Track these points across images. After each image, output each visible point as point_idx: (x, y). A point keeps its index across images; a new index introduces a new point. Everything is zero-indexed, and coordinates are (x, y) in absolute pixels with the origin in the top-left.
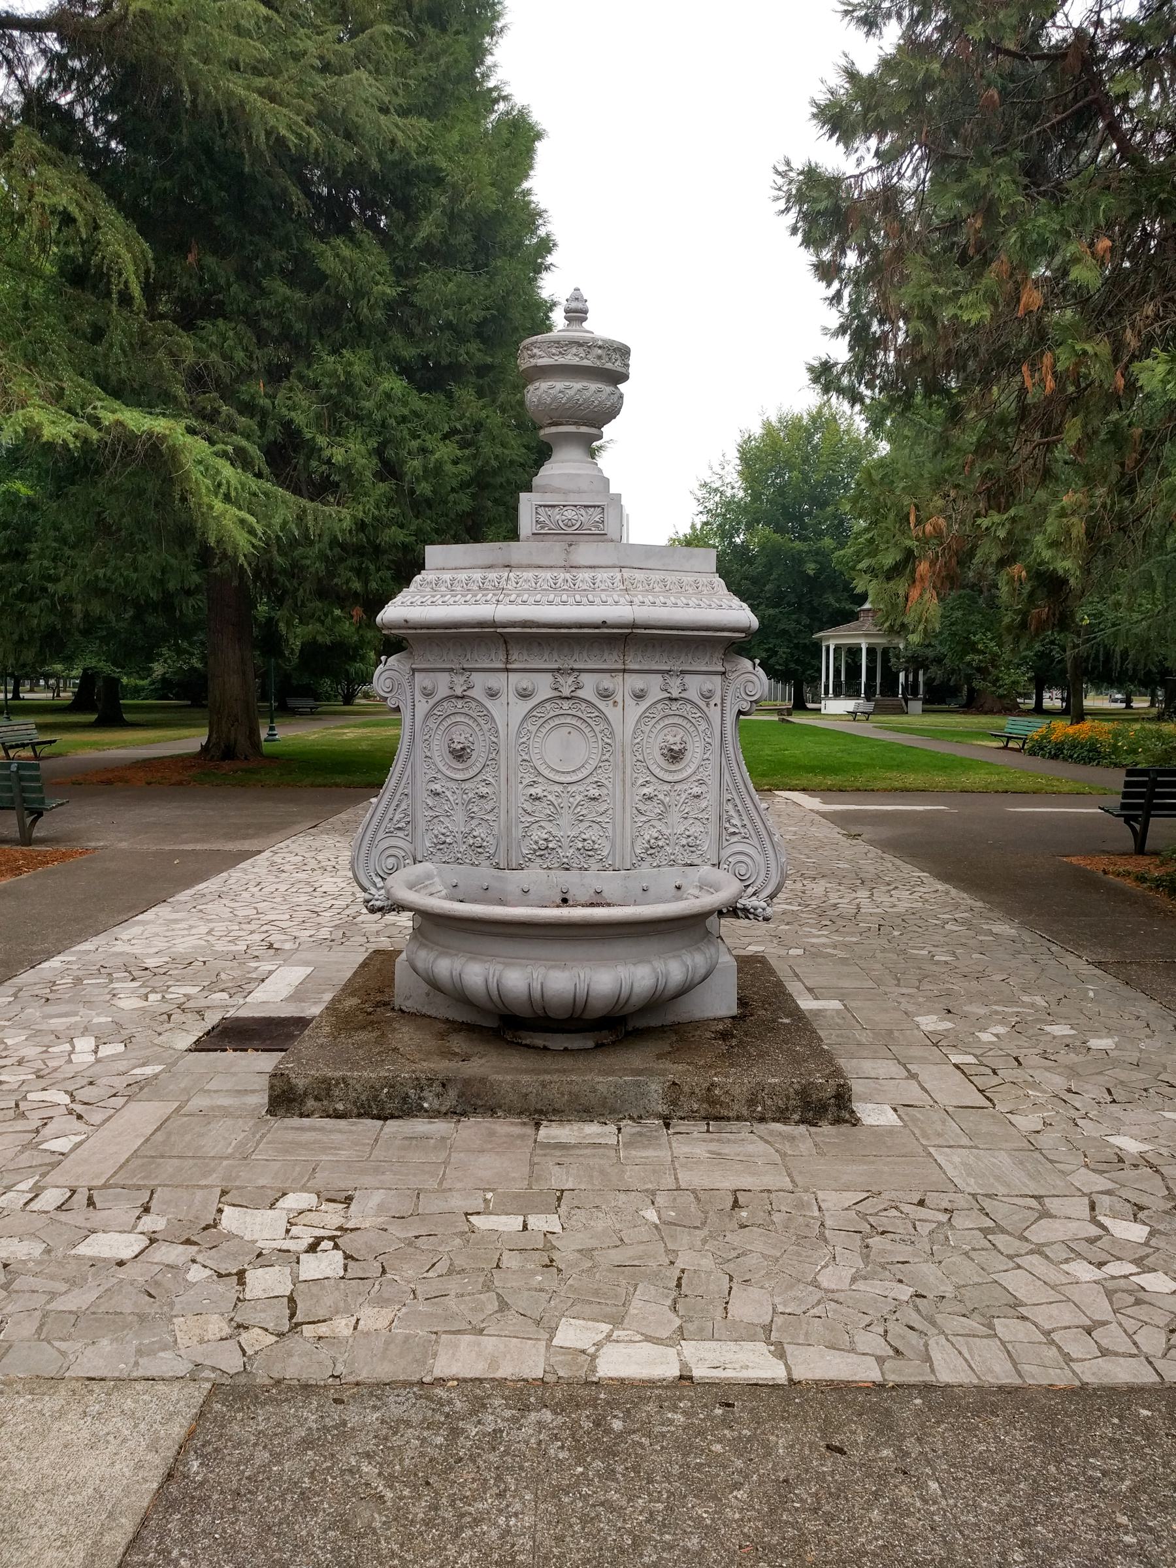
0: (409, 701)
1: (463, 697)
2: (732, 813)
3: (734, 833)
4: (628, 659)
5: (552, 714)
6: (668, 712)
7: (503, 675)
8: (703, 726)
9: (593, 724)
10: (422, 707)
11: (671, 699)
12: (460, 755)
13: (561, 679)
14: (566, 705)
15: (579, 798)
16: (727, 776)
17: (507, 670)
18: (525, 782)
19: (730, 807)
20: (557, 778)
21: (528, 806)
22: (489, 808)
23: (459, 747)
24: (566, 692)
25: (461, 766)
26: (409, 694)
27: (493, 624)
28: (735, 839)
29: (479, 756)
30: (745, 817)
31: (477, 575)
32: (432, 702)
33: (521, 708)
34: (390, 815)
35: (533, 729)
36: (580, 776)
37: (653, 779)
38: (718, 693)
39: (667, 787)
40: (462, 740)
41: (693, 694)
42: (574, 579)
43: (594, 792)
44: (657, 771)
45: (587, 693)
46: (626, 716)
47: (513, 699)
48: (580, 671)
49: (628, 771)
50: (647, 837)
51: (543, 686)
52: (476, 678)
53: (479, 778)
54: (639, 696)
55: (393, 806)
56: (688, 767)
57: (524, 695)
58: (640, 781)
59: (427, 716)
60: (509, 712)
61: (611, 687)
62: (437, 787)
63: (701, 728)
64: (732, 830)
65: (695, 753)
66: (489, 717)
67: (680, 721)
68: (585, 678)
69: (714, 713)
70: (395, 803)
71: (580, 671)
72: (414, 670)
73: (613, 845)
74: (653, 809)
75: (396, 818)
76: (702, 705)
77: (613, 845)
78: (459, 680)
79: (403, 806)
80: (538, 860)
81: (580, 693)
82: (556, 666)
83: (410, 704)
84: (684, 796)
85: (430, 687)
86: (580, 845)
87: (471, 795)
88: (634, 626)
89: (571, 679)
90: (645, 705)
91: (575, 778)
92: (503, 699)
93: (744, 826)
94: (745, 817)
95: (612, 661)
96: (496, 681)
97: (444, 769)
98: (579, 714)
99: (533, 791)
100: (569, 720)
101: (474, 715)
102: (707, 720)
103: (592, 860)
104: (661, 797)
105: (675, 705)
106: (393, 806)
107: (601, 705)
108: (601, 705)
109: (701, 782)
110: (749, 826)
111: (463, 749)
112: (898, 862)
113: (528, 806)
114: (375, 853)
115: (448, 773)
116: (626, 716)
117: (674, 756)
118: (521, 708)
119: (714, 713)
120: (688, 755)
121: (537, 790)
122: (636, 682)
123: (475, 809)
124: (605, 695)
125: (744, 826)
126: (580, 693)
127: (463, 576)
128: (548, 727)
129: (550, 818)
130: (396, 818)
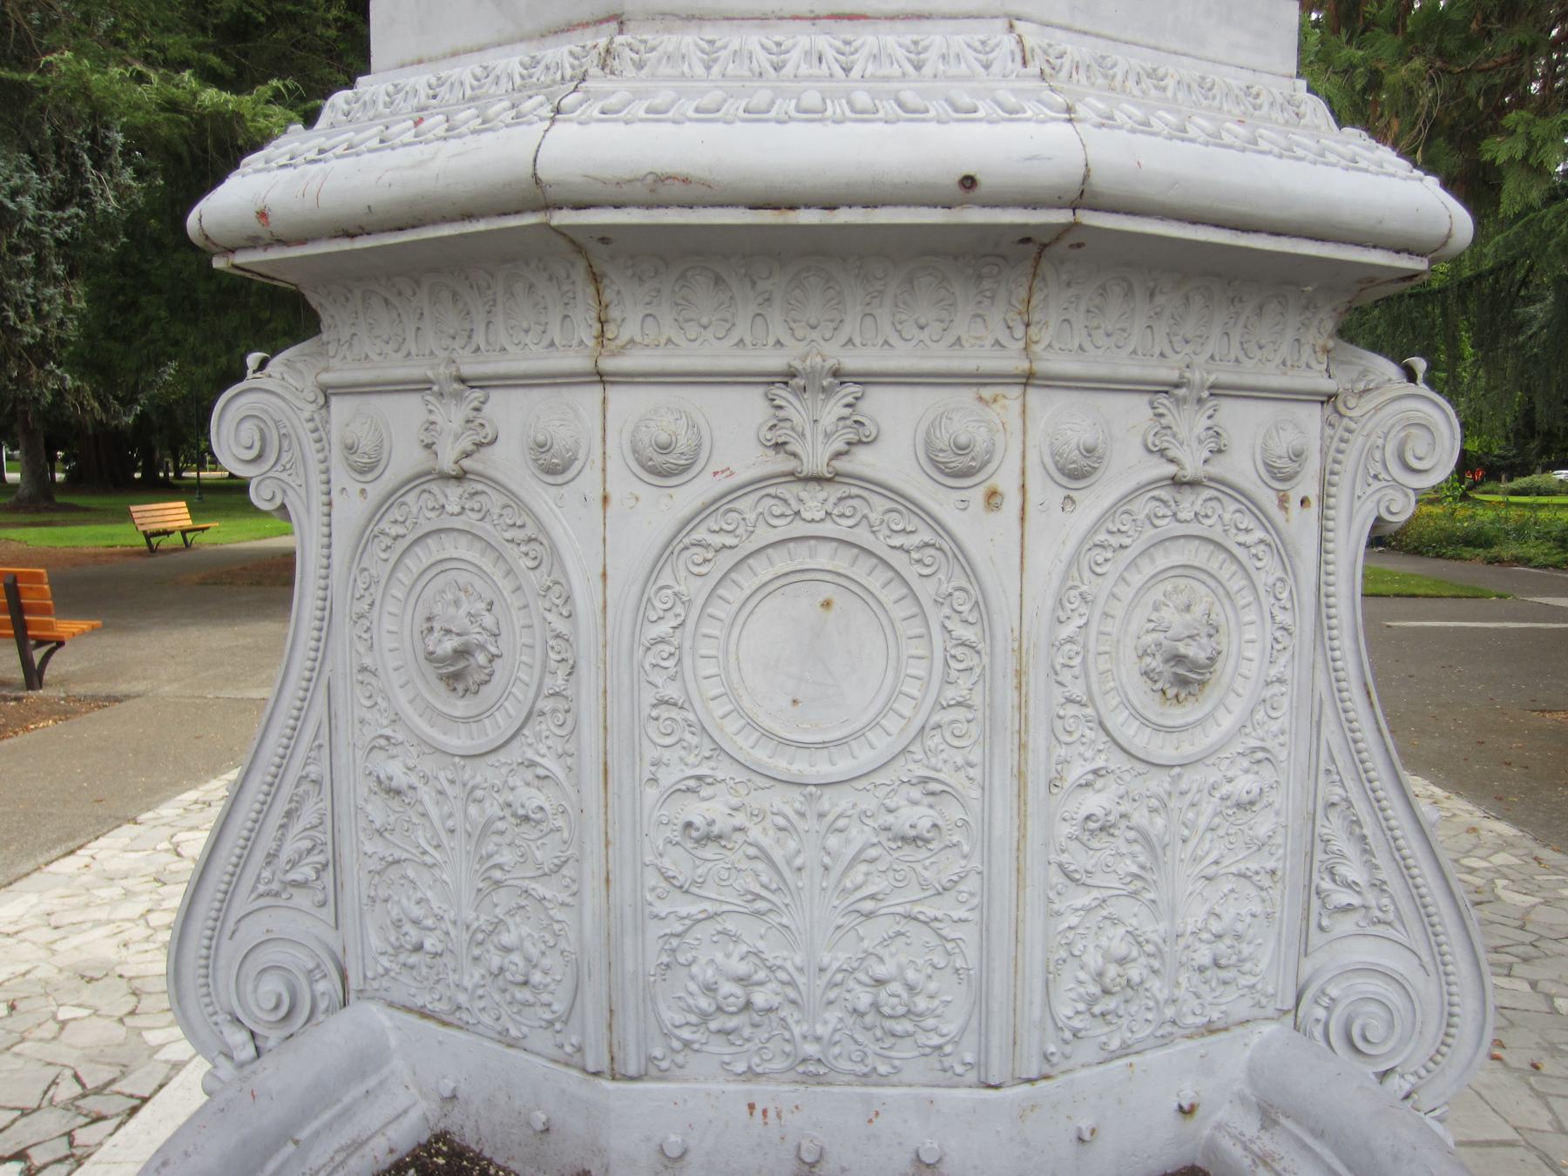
0: (317, 488)
1: (461, 477)
2: (1342, 843)
3: (1348, 908)
4: (1043, 336)
5: (765, 535)
6: (1167, 526)
7: (593, 394)
8: (1268, 570)
9: (911, 572)
10: (351, 508)
11: (1177, 483)
12: (458, 671)
13: (796, 410)
14: (814, 501)
15: (859, 835)
16: (1330, 732)
17: (601, 378)
18: (668, 777)
19: (1333, 828)
20: (782, 764)
21: (678, 862)
22: (544, 855)
23: (449, 645)
24: (815, 457)
25: (460, 707)
26: (314, 467)
27: (538, 195)
28: (1347, 924)
29: (517, 676)
30: (1382, 859)
31: (510, 61)
32: (376, 491)
33: (655, 512)
34: (266, 843)
35: (696, 589)
36: (864, 757)
37: (1117, 761)
38: (1313, 463)
39: (1158, 783)
40: (459, 618)
41: (1241, 467)
42: (847, 50)
43: (918, 816)
44: (1130, 733)
45: (892, 459)
46: (1027, 550)
47: (624, 482)
48: (868, 379)
49: (1038, 737)
50: (1093, 960)
51: (733, 428)
52: (506, 409)
53: (515, 753)
54: (1077, 471)
55: (275, 818)
56: (1220, 716)
57: (664, 466)
58: (1077, 772)
59: (366, 536)
60: (606, 531)
61: (981, 438)
62: (395, 770)
63: (1262, 579)
64: (1343, 897)
65: (1248, 653)
66: (539, 542)
67: (1198, 555)
68: (882, 405)
69: (1301, 526)
70: (281, 806)
71: (868, 379)
72: (328, 392)
73: (982, 999)
74: (1114, 860)
75: (288, 852)
76: (1268, 500)
77: (982, 999)
78: (451, 417)
79: (308, 816)
80: (718, 1046)
81: (864, 461)
82: (774, 361)
83: (318, 499)
84: (1208, 809)
85: (366, 443)
86: (864, 999)
87: (493, 809)
88: (1083, 197)
89: (832, 410)
90: (1095, 500)
91: (843, 766)
92: (589, 483)
93: (1379, 886)
94: (1382, 859)
95: (981, 337)
96: (571, 416)
97: (410, 713)
98: (862, 536)
99: (696, 811)
100: (824, 558)
101: (497, 536)
102: (1282, 550)
103: (905, 1050)
104: (1140, 817)
105: (1190, 504)
106: (275, 818)
107: (941, 502)
108: (941, 502)
109: (1261, 757)
110: (1395, 885)
111: (463, 653)
112: (1438, 791)
113: (678, 862)
114: (230, 952)
115: (422, 725)
116: (1027, 550)
117: (1184, 676)
118: (655, 512)
119: (1301, 526)
120: (1225, 668)
121: (709, 809)
122: (1062, 420)
123: (506, 857)
124: (957, 466)
125: (1379, 886)
126: (864, 461)
127: (464, 71)
128: (748, 581)
129: (756, 907)
130: (288, 852)
